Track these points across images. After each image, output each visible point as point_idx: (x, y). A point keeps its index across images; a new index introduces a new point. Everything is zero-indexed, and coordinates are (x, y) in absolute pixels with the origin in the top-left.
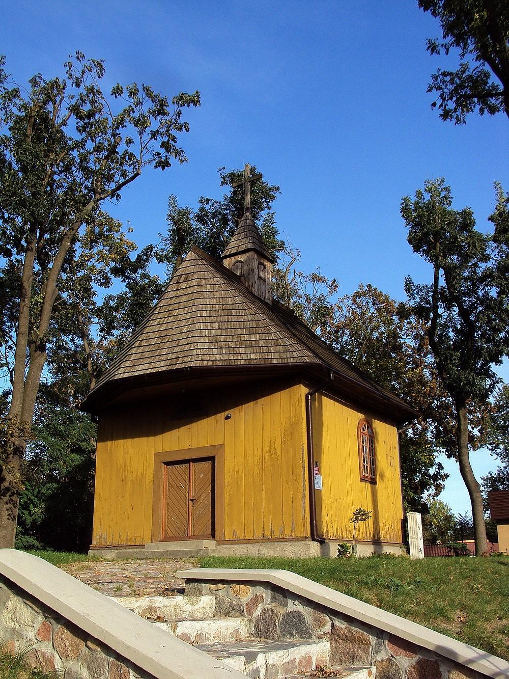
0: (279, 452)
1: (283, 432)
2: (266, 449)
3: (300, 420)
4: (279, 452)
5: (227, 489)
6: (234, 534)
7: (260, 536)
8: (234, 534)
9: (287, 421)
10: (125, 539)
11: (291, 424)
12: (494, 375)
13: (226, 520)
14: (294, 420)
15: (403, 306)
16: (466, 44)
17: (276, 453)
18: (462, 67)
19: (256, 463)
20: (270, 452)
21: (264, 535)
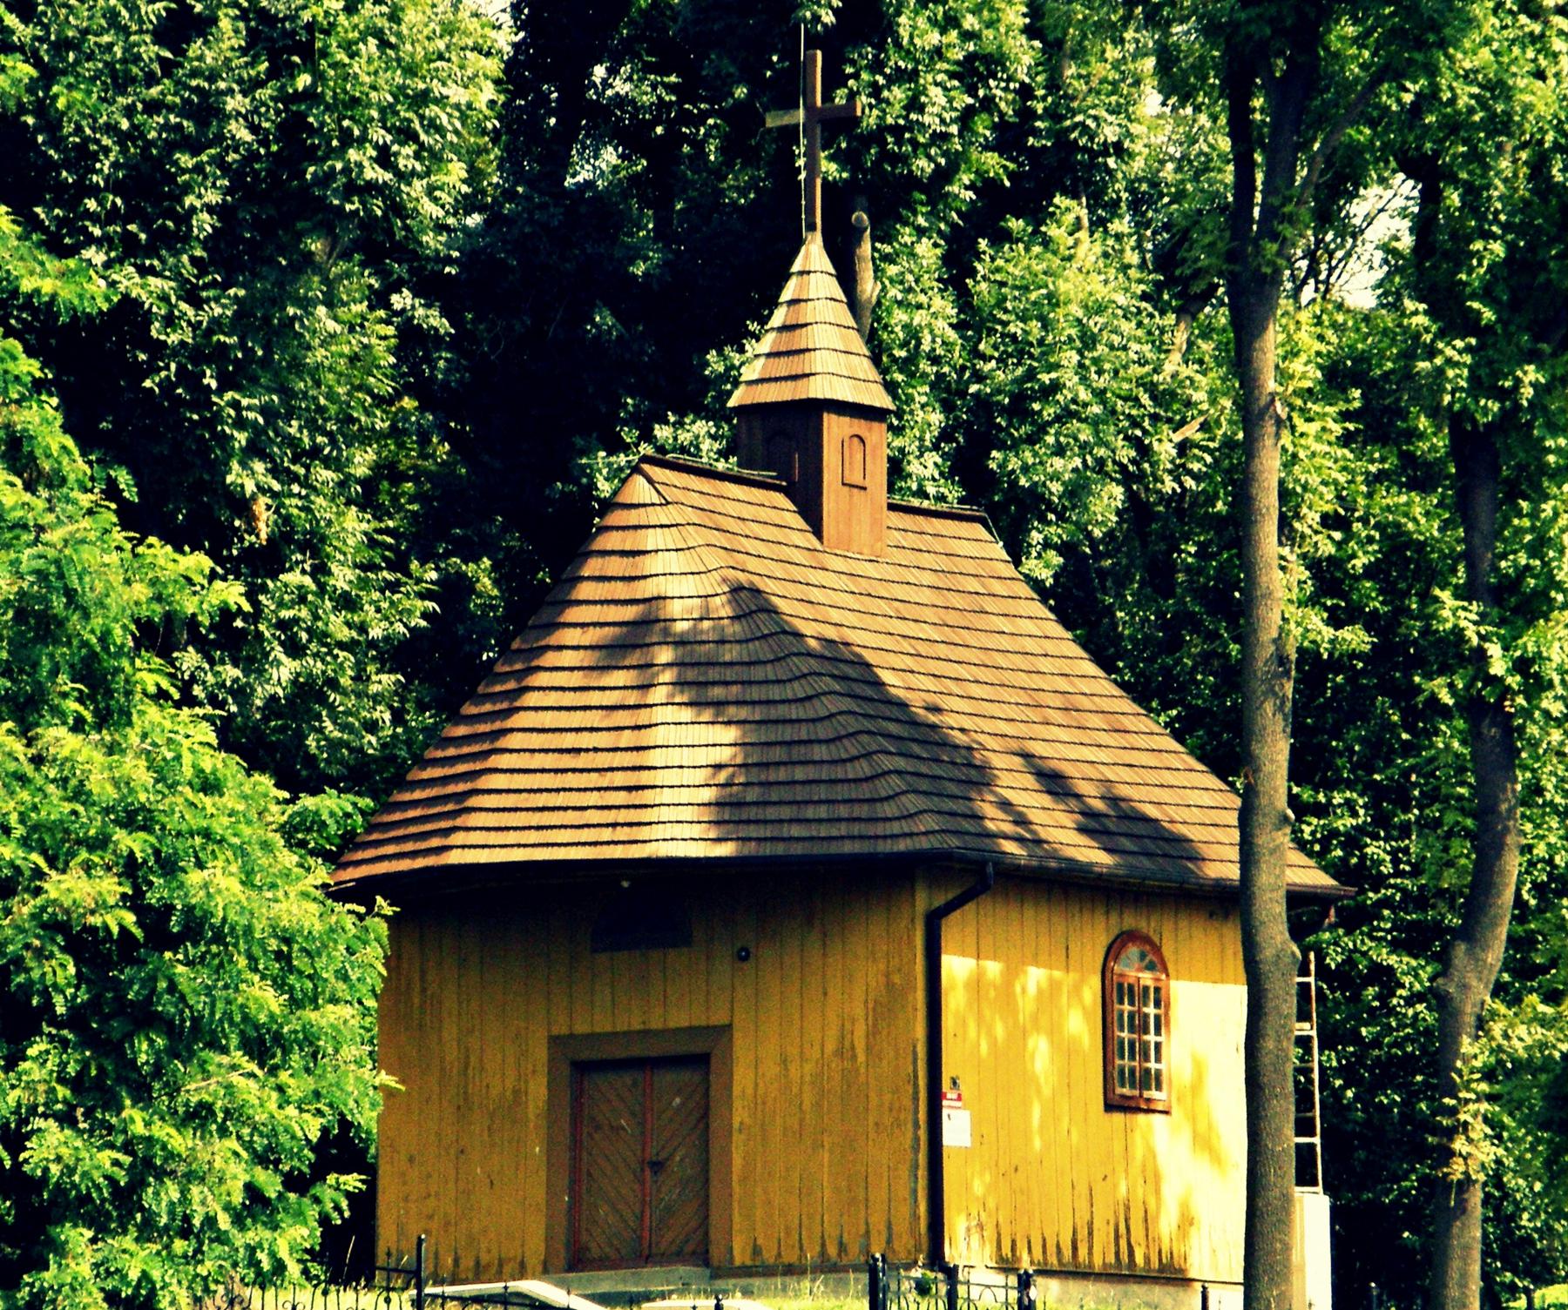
0: (861, 1058)
1: (871, 1006)
2: (830, 1047)
3: (909, 978)
4: (861, 1058)
5: (738, 1139)
6: (756, 1251)
7: (810, 1256)
8: (756, 1251)
9: (882, 980)
10: (472, 1264)
11: (889, 985)
12: (1325, 869)
13: (737, 1218)
14: (897, 979)
15: (1299, 122)
16: (312, 1149)
17: (854, 1057)
18: (1532, 864)
19: (808, 1078)
20: (839, 1052)
21: (823, 1253)
